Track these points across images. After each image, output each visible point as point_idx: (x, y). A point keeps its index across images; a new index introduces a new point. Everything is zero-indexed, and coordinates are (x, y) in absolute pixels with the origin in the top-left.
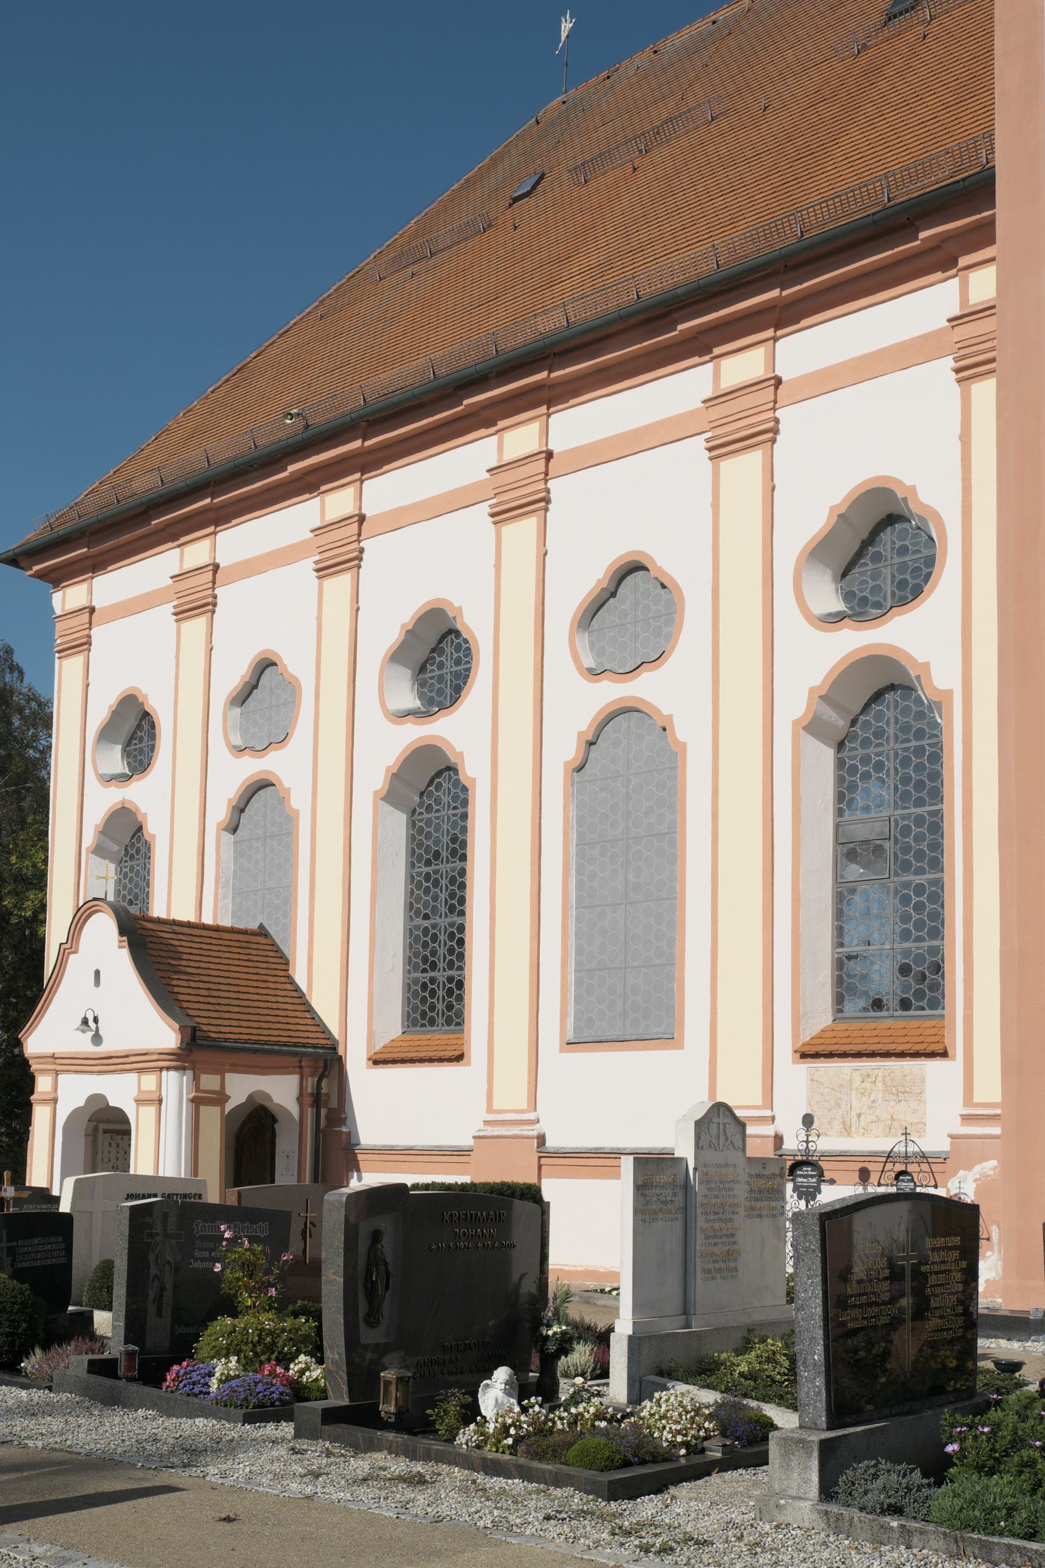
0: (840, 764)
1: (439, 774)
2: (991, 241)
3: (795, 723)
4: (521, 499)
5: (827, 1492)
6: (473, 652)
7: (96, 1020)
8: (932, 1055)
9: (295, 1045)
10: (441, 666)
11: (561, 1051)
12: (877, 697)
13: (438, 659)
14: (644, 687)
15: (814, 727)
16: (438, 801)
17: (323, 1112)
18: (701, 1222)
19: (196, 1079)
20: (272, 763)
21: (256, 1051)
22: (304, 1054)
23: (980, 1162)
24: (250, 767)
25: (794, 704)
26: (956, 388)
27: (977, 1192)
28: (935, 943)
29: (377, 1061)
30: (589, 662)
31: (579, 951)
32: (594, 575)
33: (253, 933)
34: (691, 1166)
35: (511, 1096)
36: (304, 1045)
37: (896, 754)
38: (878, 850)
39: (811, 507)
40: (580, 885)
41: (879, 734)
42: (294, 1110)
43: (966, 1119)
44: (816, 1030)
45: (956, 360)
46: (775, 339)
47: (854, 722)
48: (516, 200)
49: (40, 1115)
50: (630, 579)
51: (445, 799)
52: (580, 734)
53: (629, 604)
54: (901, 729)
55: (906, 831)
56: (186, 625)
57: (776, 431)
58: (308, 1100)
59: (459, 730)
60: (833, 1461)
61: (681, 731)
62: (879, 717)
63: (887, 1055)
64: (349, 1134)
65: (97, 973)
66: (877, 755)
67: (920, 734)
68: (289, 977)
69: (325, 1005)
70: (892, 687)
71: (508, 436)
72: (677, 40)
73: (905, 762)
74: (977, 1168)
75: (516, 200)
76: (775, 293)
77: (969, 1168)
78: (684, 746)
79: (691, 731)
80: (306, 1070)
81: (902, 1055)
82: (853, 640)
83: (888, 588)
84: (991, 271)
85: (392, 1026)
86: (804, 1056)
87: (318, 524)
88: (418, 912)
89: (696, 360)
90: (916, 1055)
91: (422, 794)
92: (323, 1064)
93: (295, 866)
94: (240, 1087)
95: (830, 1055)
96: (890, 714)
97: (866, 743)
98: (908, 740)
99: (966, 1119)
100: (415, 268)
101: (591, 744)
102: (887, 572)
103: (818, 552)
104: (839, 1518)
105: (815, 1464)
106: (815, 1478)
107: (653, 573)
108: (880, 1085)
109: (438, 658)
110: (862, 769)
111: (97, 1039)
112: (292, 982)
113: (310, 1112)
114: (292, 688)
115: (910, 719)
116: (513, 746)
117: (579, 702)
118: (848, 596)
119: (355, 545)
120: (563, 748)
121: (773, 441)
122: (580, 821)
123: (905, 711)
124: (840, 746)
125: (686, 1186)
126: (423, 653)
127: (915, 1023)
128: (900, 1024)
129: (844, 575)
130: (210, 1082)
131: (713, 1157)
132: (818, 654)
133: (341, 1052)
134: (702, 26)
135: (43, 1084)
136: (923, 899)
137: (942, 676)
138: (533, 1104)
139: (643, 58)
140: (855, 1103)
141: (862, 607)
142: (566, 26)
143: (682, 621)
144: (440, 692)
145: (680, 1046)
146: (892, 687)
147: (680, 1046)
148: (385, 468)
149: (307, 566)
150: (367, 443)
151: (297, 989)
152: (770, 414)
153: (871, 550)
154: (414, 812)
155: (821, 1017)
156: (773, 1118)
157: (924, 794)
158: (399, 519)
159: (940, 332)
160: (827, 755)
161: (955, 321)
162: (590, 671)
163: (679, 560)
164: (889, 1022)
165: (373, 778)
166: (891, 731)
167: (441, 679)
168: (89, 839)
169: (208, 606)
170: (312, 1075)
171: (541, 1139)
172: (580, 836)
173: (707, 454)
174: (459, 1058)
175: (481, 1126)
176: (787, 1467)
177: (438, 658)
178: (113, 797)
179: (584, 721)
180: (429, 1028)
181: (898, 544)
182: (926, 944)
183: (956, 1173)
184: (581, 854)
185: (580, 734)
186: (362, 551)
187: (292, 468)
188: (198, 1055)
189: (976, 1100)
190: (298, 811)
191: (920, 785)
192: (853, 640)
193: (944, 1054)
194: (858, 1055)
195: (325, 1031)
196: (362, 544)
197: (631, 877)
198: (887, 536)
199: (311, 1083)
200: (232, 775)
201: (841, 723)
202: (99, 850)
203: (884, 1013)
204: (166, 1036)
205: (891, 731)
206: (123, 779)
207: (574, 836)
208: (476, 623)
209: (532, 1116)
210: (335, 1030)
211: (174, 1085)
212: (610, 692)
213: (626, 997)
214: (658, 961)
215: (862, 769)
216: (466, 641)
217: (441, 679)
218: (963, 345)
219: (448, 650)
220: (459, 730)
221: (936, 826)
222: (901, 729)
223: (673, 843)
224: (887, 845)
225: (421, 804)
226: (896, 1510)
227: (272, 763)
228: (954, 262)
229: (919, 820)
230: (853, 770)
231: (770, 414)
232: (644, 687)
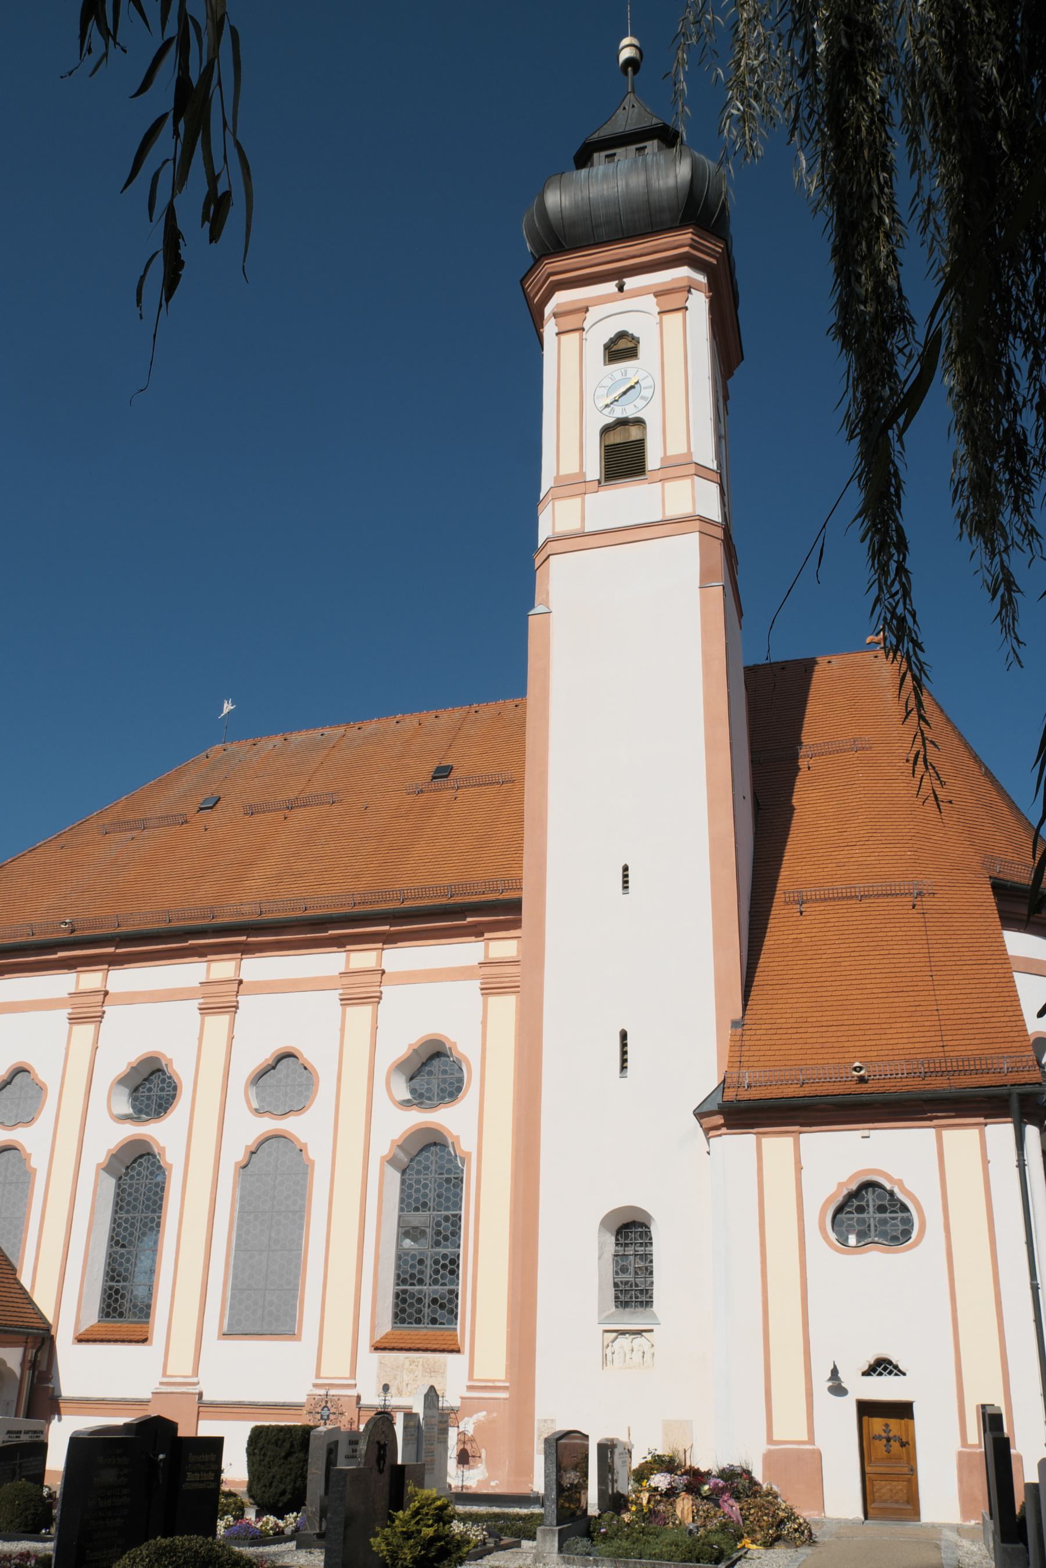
0: (403, 1182)
1: (141, 1156)
2: (520, 927)
3: (382, 1158)
4: (220, 1002)
5: (560, 1550)
6: (611, 1292)
8: (452, 1351)
9: (27, 1327)
10: (150, 1090)
11: (219, 1339)
12: (426, 1148)
13: (148, 1086)
14: (290, 1125)
15: (392, 1161)
16: (139, 1174)
18: (424, 1446)
21: (6, 1332)
22: (28, 1334)
23: (477, 1412)
25: (382, 1146)
26: (481, 998)
27: (475, 1430)
28: (452, 1287)
29: (81, 1340)
30: (255, 1105)
31: (235, 1277)
32: (265, 1055)
34: (421, 1417)
35: (181, 1366)
36: (32, 1328)
37: (435, 1181)
38: (423, 1233)
39: (399, 1041)
40: (239, 1237)
41: (426, 1168)
42: (17, 1371)
43: (470, 1388)
44: (384, 1333)
45: (482, 984)
46: (383, 949)
47: (412, 1160)
48: (201, 809)
50: (285, 1061)
51: (144, 1173)
52: (247, 1147)
53: (283, 1077)
54: (439, 1167)
55: (438, 1224)
57: (380, 998)
58: (28, 1365)
59: (164, 1133)
60: (563, 1537)
61: (312, 1153)
62: (427, 1158)
63: (426, 1350)
64: (53, 1389)
66: (425, 1179)
67: (449, 1171)
68: (16, 1279)
69: (44, 1301)
70: (435, 1144)
71: (213, 965)
72: (298, 738)
73: (440, 1186)
74: (475, 1416)
75: (201, 809)
76: (387, 928)
77: (470, 1416)
78: (313, 1162)
79: (318, 1153)
80: (30, 1345)
81: (434, 1351)
82: (417, 1118)
83: (436, 1090)
85: (92, 1317)
86: (377, 1349)
87: (73, 991)
88: (117, 1243)
89: (335, 949)
90: (443, 1351)
91: (127, 1168)
92: (40, 1341)
93: (29, 1205)
95: (393, 1349)
96: (432, 1158)
97: (418, 1172)
98: (442, 1174)
99: (470, 1388)
100: (135, 833)
101: (253, 1153)
102: (435, 1082)
103: (400, 1066)
104: (569, 1559)
105: (556, 1539)
106: (556, 1544)
107: (301, 1061)
108: (420, 1367)
109: (151, 1087)
110: (415, 1186)
112: (18, 1283)
113: (28, 1373)
114: (41, 1089)
115: (444, 1162)
116: (201, 1149)
117: (247, 1128)
118: (413, 1091)
119: (99, 1009)
120: (235, 1153)
121: (379, 1003)
122: (242, 1198)
123: (442, 1158)
124: (403, 1172)
125: (419, 1427)
126: (139, 1080)
127: (439, 1333)
128: (431, 1332)
129: (411, 1079)
131: (430, 1413)
132: (398, 1122)
133: (53, 1333)
134: (315, 734)
136: (447, 1262)
137: (466, 1143)
138: (196, 1372)
139: (277, 740)
140: (405, 1378)
141: (420, 1099)
142: (228, 707)
143: (317, 1091)
144: (148, 1106)
145: (299, 1339)
146: (435, 1144)
147: (299, 1339)
148: (126, 966)
149: (64, 1013)
150: (118, 951)
151: (22, 1288)
152: (377, 989)
153: (427, 1068)
154: (120, 1178)
155: (386, 1325)
156: (356, 1385)
157: (450, 1204)
158: (132, 998)
159: (473, 967)
160: (397, 1176)
161: (482, 964)
162: (256, 1110)
163: (316, 1053)
164: (425, 1331)
166: (433, 1167)
167: (149, 1098)
170: (33, 1348)
171: (201, 1395)
172: (242, 1207)
173: (339, 1002)
174: (144, 1341)
175: (158, 1385)
176: (544, 1541)
177: (151, 1087)
179: (250, 1139)
180: (118, 1319)
181: (443, 1068)
182: (447, 1288)
183: (463, 1419)
184: (241, 1218)
185: (247, 1147)
186: (104, 1012)
187: (60, 954)
189: (475, 1377)
190: (35, 1170)
191: (448, 1199)
192: (417, 1118)
193: (458, 1351)
194: (409, 1350)
195: (42, 1317)
196: (104, 1008)
197: (273, 1235)
198: (436, 1062)
199: (31, 1353)
201: (406, 1160)
203: (421, 1326)
205: (433, 1167)
207: (237, 1206)
208: (181, 1069)
209: (195, 1380)
210: (50, 1318)
212: (268, 1125)
213: (263, 1305)
214: (286, 1287)
215: (415, 1186)
216: (170, 1078)
217: (149, 1098)
218: (484, 977)
219: (156, 1081)
220: (164, 1133)
221: (456, 1221)
222: (439, 1167)
223: (302, 1218)
224: (428, 1230)
225: (126, 1174)
226: (589, 1554)
228: (483, 935)
229: (446, 1219)
230: (410, 1186)
231: (377, 989)
232: (290, 1125)
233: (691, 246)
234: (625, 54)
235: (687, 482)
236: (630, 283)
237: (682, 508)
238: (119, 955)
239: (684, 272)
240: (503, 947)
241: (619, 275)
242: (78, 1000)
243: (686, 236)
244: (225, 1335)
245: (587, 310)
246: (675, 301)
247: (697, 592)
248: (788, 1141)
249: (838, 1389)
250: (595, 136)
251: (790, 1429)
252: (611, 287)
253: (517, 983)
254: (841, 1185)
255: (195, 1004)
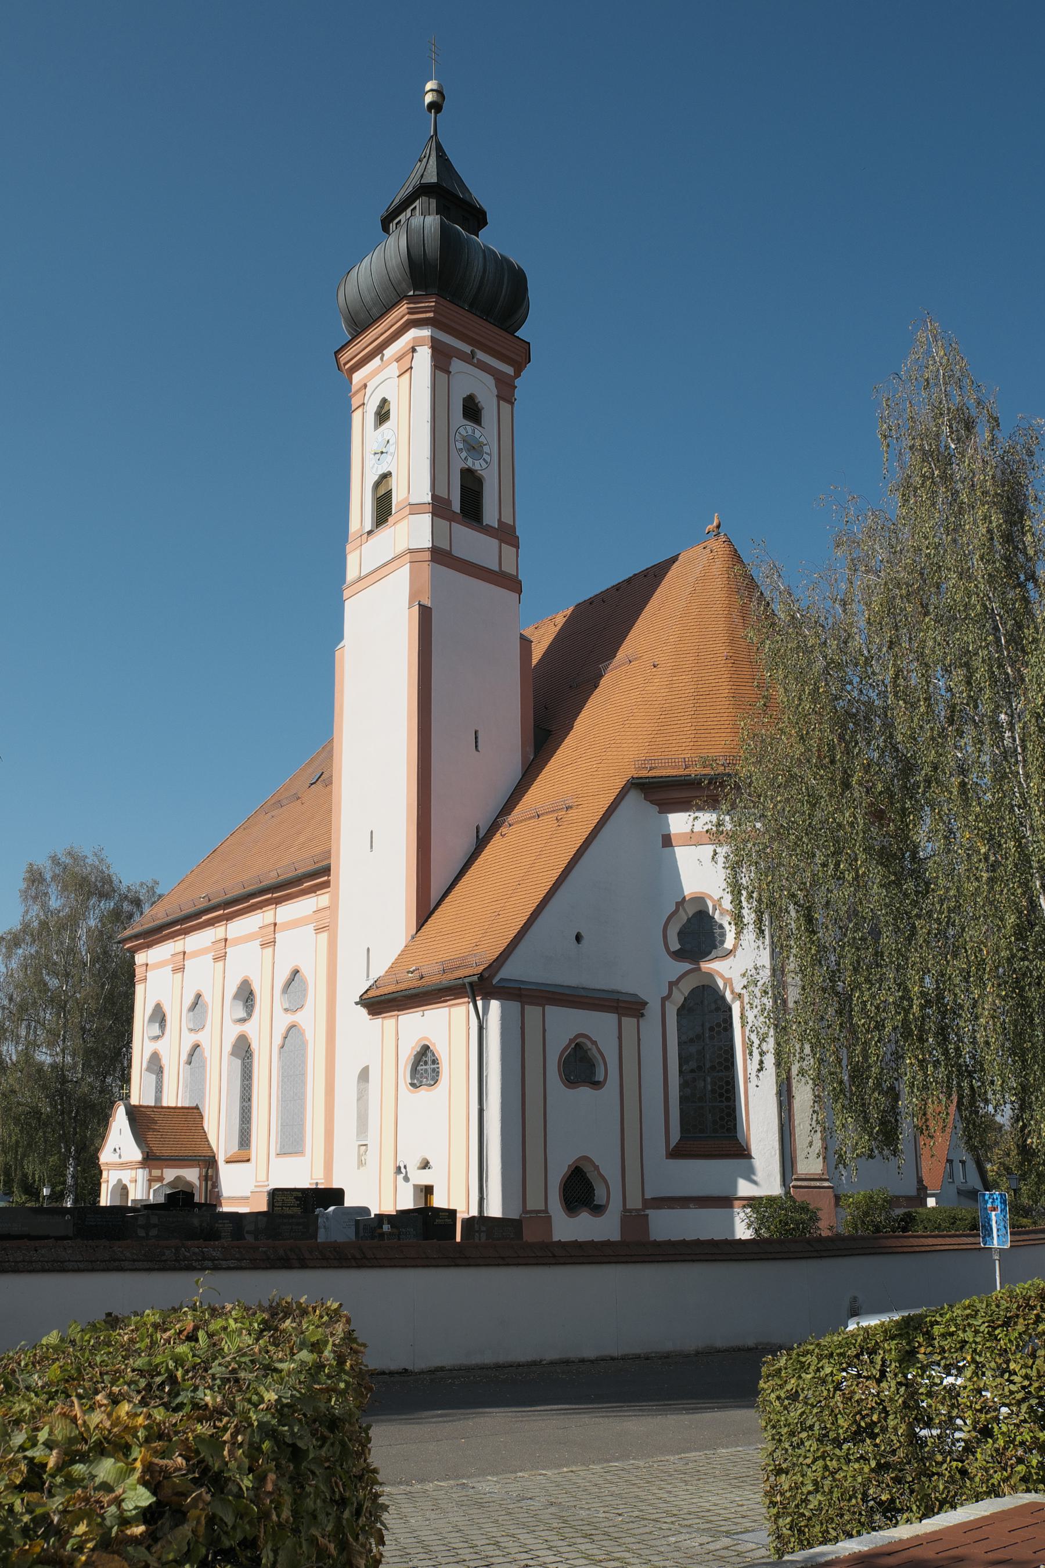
2: (329, 887)
7: (119, 1149)
17: (209, 1183)
19: (150, 1172)
20: (298, 1018)
24: (290, 1018)
33: (192, 1108)
49: (104, 1187)
56: (319, 935)
65: (476, 732)
84: (327, 895)
85: (234, 1147)
92: (209, 1163)
94: (170, 1174)
111: (120, 1156)
130: (156, 1173)
135: (105, 1174)
149: (210, 956)
165: (228, 1048)
168: (145, 1066)
169: (182, 969)
174: (248, 1160)
178: (239, 1029)
187: (204, 918)
188: (149, 1162)
200: (282, 1021)
202: (148, 1069)
204: (137, 1155)
206: (243, 1020)
211: (142, 1174)
227: (298, 1018)
233: (409, 313)
234: (429, 98)
235: (405, 521)
236: (390, 352)
237: (402, 546)
238: (276, 898)
239: (413, 333)
240: (322, 899)
241: (379, 350)
242: (320, 915)
243: (403, 308)
244: (676, 1153)
245: (365, 386)
246: (405, 363)
247: (407, 611)
248: (393, 1021)
249: (406, 1179)
250: (397, 200)
251: (535, 1203)
252: (376, 362)
253: (326, 924)
254: (413, 1048)
255: (311, 927)
